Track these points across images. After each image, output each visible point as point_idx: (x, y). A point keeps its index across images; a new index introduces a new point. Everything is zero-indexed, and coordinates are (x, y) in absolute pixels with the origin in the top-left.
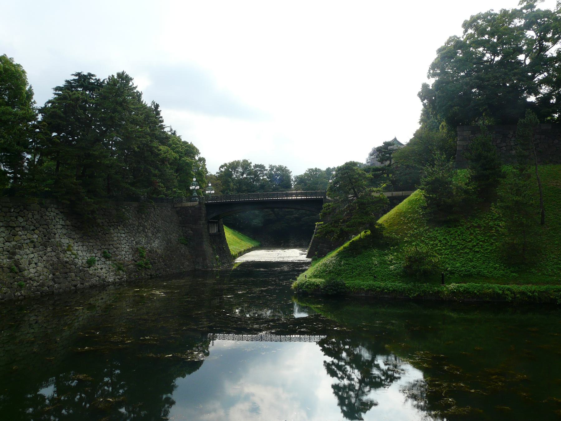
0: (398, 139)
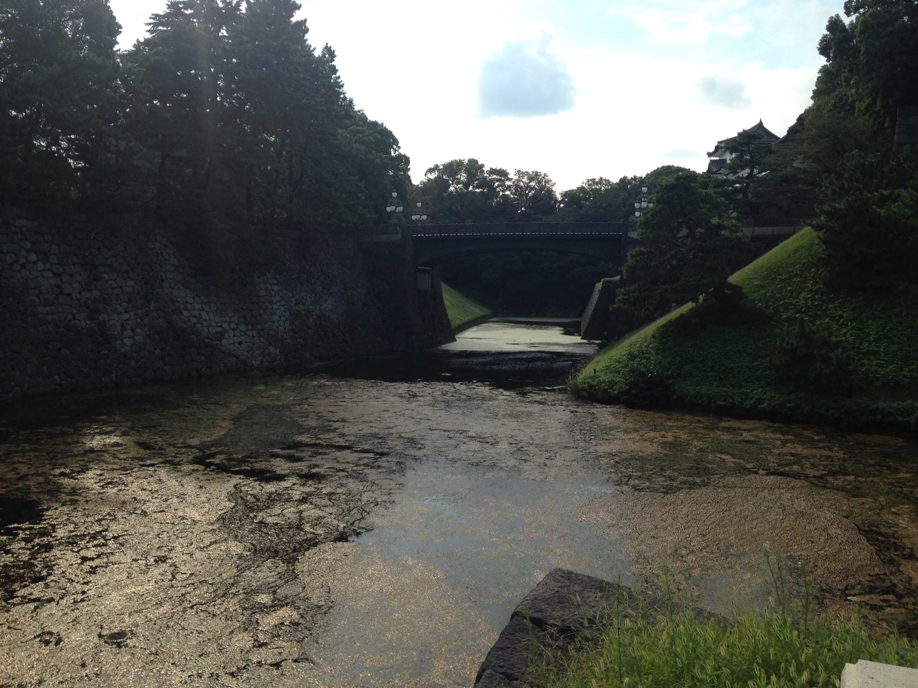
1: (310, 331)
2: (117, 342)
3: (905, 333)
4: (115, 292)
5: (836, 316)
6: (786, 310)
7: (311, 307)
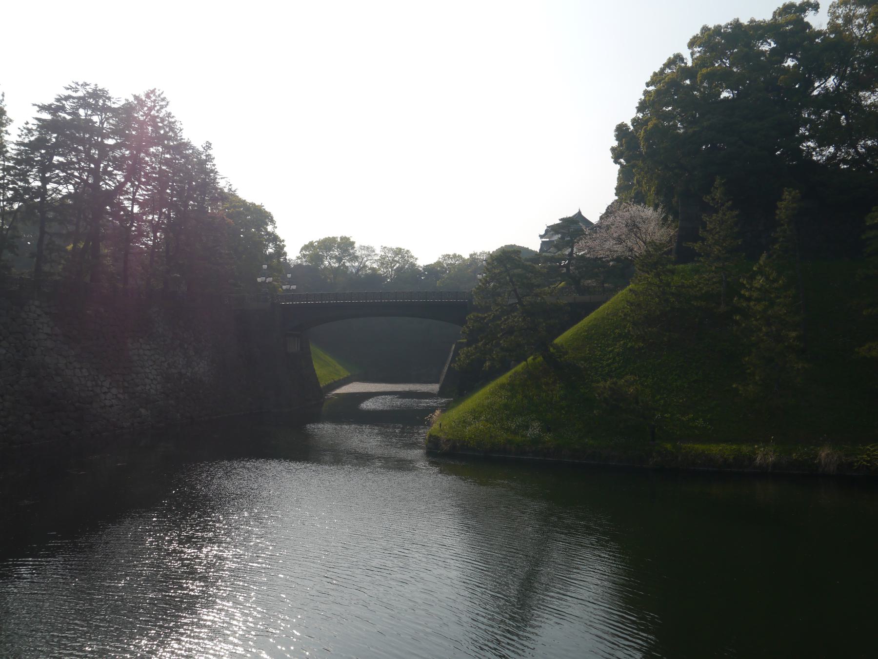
0: (583, 214)
7: (183, 371)
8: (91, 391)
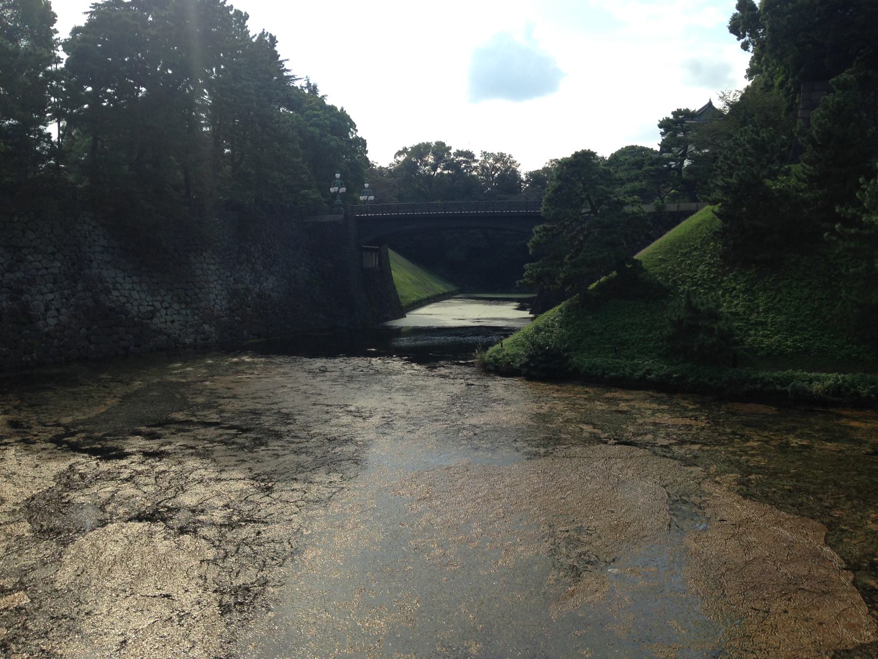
1: (248, 309)
2: (40, 322)
3: (793, 303)
4: (40, 273)
5: (729, 289)
6: (684, 283)
7: (251, 286)
8: (152, 306)
